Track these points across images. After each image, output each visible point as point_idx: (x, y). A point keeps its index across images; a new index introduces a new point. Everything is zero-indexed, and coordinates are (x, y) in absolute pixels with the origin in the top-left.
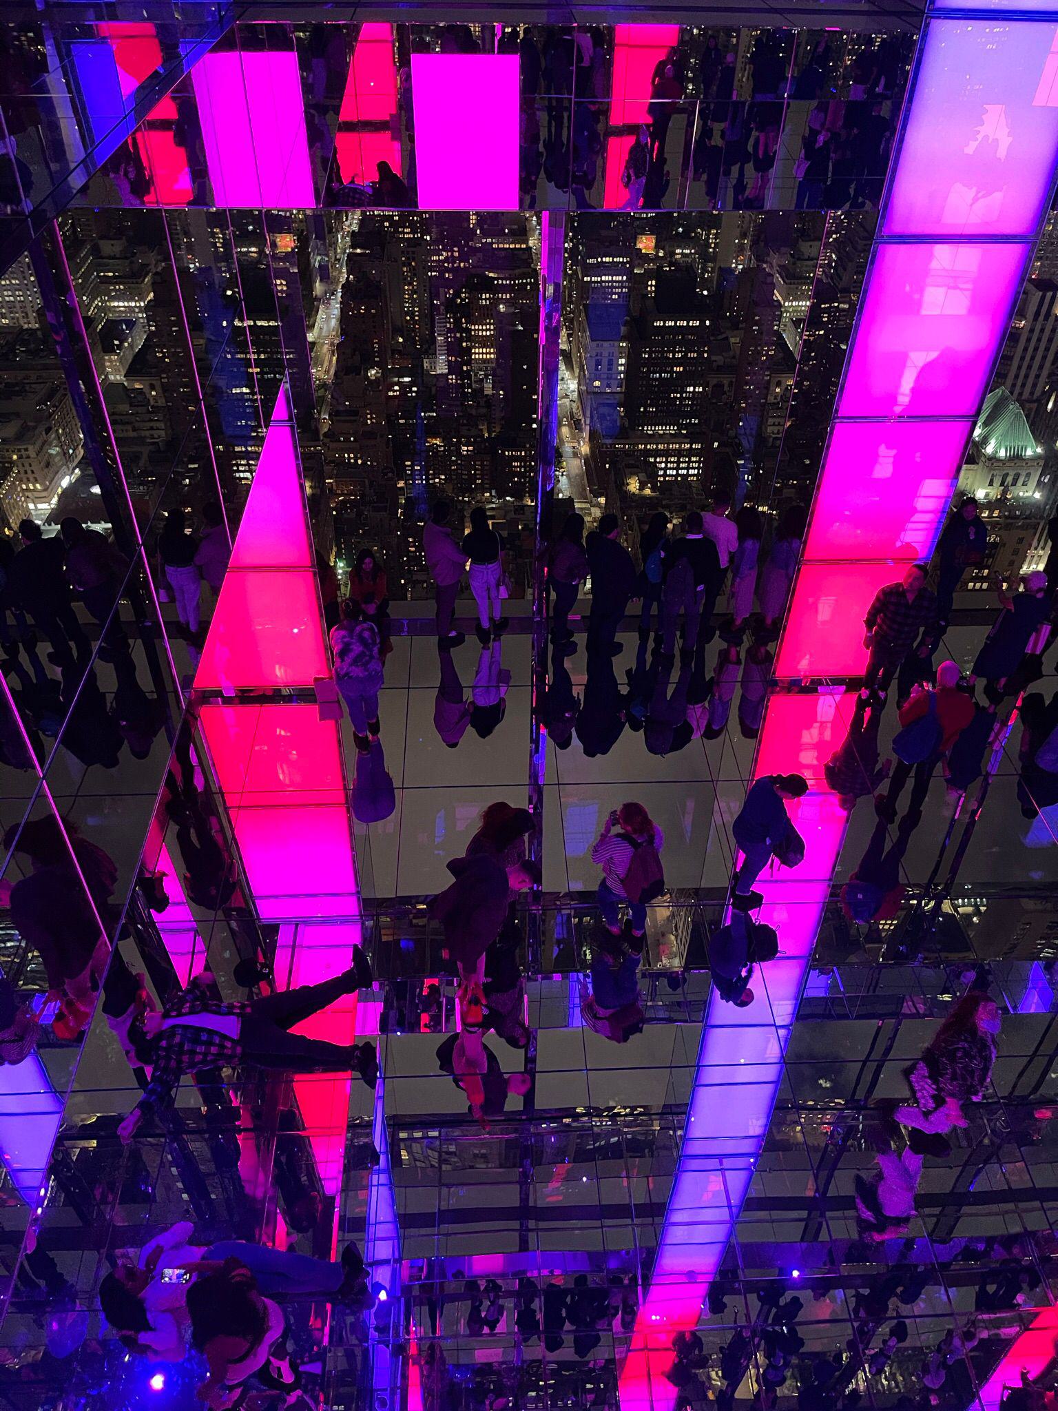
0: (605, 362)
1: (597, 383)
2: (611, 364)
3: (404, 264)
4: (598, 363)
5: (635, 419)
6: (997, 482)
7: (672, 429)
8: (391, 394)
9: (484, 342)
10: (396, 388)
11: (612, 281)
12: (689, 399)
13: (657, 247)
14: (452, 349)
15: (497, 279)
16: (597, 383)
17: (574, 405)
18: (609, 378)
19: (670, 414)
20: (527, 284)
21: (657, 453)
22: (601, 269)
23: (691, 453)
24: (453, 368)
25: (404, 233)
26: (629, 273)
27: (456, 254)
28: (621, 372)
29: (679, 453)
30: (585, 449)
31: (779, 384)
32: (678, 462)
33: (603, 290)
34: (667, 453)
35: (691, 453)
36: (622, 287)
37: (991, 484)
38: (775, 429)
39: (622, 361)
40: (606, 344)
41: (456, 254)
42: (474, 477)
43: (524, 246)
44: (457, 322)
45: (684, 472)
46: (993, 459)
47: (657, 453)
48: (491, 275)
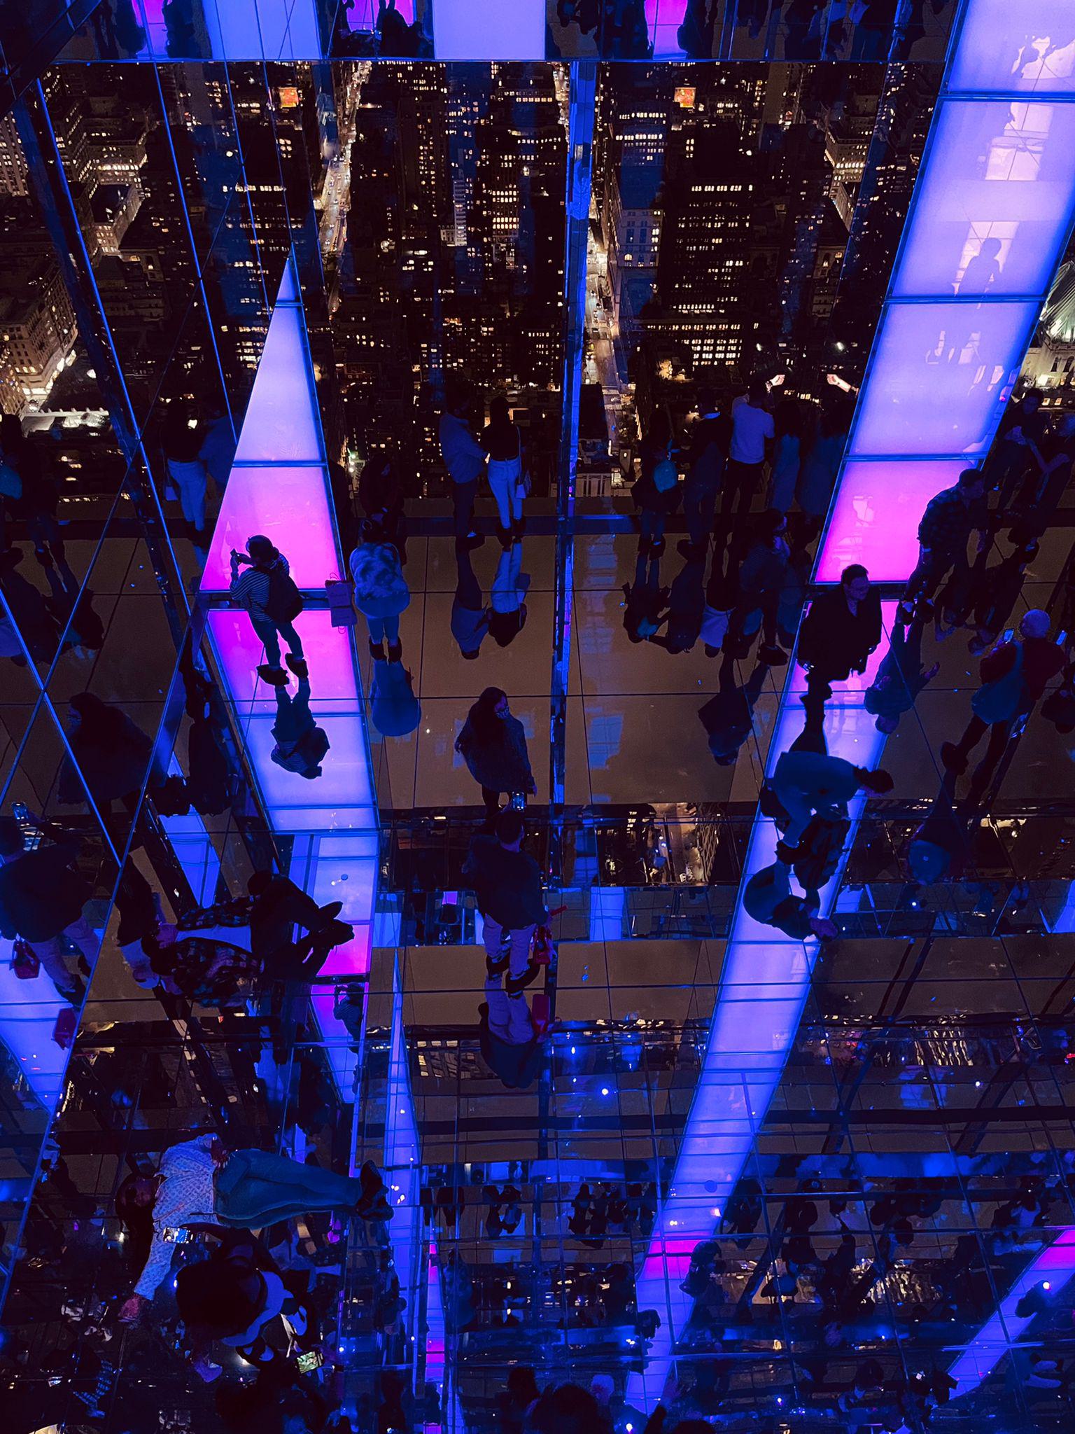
0: (637, 232)
1: (628, 257)
2: (645, 235)
3: (419, 121)
4: (630, 233)
5: (670, 297)
6: (1061, 366)
7: (709, 309)
8: (405, 268)
9: (506, 210)
10: (411, 262)
11: (647, 141)
12: (728, 274)
13: (697, 102)
14: (473, 218)
15: (520, 138)
16: (628, 257)
17: (604, 282)
18: (641, 253)
19: (706, 292)
20: (553, 143)
21: (692, 335)
22: (636, 125)
23: (729, 334)
24: (473, 239)
25: (419, 85)
26: (666, 130)
27: (476, 110)
28: (655, 244)
29: (716, 335)
30: (614, 330)
31: (827, 258)
32: (715, 345)
33: (637, 150)
34: (703, 335)
35: (729, 334)
36: (657, 147)
37: (1054, 369)
38: (821, 308)
39: (656, 232)
40: (638, 212)
41: (476, 110)
42: (495, 361)
43: (550, 100)
44: (477, 188)
45: (722, 356)
46: (1058, 341)
47: (692, 335)
48: (514, 133)
